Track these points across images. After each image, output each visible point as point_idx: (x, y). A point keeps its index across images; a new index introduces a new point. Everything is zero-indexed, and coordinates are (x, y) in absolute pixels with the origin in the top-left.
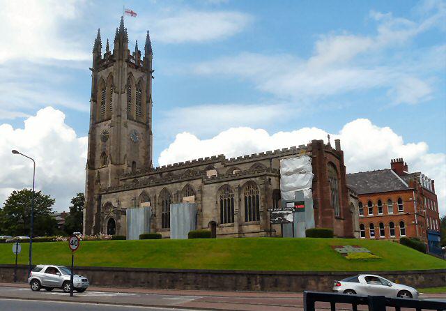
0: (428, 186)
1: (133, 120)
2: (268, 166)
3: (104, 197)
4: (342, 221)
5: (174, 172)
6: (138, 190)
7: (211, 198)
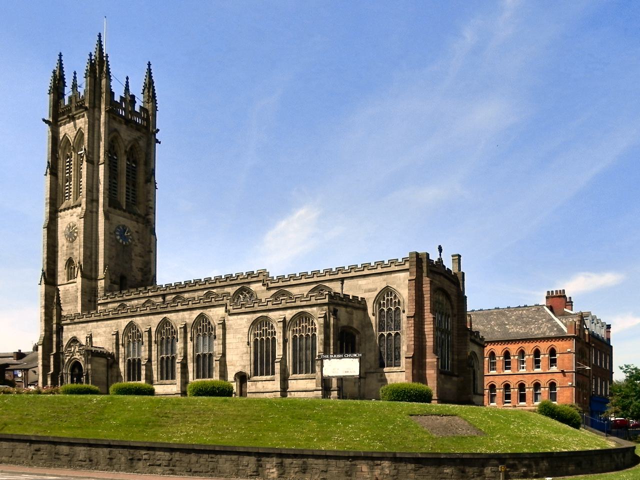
0: (602, 333)
1: (120, 208)
2: (338, 290)
4: (455, 379)
5: (186, 295)
6: (122, 320)
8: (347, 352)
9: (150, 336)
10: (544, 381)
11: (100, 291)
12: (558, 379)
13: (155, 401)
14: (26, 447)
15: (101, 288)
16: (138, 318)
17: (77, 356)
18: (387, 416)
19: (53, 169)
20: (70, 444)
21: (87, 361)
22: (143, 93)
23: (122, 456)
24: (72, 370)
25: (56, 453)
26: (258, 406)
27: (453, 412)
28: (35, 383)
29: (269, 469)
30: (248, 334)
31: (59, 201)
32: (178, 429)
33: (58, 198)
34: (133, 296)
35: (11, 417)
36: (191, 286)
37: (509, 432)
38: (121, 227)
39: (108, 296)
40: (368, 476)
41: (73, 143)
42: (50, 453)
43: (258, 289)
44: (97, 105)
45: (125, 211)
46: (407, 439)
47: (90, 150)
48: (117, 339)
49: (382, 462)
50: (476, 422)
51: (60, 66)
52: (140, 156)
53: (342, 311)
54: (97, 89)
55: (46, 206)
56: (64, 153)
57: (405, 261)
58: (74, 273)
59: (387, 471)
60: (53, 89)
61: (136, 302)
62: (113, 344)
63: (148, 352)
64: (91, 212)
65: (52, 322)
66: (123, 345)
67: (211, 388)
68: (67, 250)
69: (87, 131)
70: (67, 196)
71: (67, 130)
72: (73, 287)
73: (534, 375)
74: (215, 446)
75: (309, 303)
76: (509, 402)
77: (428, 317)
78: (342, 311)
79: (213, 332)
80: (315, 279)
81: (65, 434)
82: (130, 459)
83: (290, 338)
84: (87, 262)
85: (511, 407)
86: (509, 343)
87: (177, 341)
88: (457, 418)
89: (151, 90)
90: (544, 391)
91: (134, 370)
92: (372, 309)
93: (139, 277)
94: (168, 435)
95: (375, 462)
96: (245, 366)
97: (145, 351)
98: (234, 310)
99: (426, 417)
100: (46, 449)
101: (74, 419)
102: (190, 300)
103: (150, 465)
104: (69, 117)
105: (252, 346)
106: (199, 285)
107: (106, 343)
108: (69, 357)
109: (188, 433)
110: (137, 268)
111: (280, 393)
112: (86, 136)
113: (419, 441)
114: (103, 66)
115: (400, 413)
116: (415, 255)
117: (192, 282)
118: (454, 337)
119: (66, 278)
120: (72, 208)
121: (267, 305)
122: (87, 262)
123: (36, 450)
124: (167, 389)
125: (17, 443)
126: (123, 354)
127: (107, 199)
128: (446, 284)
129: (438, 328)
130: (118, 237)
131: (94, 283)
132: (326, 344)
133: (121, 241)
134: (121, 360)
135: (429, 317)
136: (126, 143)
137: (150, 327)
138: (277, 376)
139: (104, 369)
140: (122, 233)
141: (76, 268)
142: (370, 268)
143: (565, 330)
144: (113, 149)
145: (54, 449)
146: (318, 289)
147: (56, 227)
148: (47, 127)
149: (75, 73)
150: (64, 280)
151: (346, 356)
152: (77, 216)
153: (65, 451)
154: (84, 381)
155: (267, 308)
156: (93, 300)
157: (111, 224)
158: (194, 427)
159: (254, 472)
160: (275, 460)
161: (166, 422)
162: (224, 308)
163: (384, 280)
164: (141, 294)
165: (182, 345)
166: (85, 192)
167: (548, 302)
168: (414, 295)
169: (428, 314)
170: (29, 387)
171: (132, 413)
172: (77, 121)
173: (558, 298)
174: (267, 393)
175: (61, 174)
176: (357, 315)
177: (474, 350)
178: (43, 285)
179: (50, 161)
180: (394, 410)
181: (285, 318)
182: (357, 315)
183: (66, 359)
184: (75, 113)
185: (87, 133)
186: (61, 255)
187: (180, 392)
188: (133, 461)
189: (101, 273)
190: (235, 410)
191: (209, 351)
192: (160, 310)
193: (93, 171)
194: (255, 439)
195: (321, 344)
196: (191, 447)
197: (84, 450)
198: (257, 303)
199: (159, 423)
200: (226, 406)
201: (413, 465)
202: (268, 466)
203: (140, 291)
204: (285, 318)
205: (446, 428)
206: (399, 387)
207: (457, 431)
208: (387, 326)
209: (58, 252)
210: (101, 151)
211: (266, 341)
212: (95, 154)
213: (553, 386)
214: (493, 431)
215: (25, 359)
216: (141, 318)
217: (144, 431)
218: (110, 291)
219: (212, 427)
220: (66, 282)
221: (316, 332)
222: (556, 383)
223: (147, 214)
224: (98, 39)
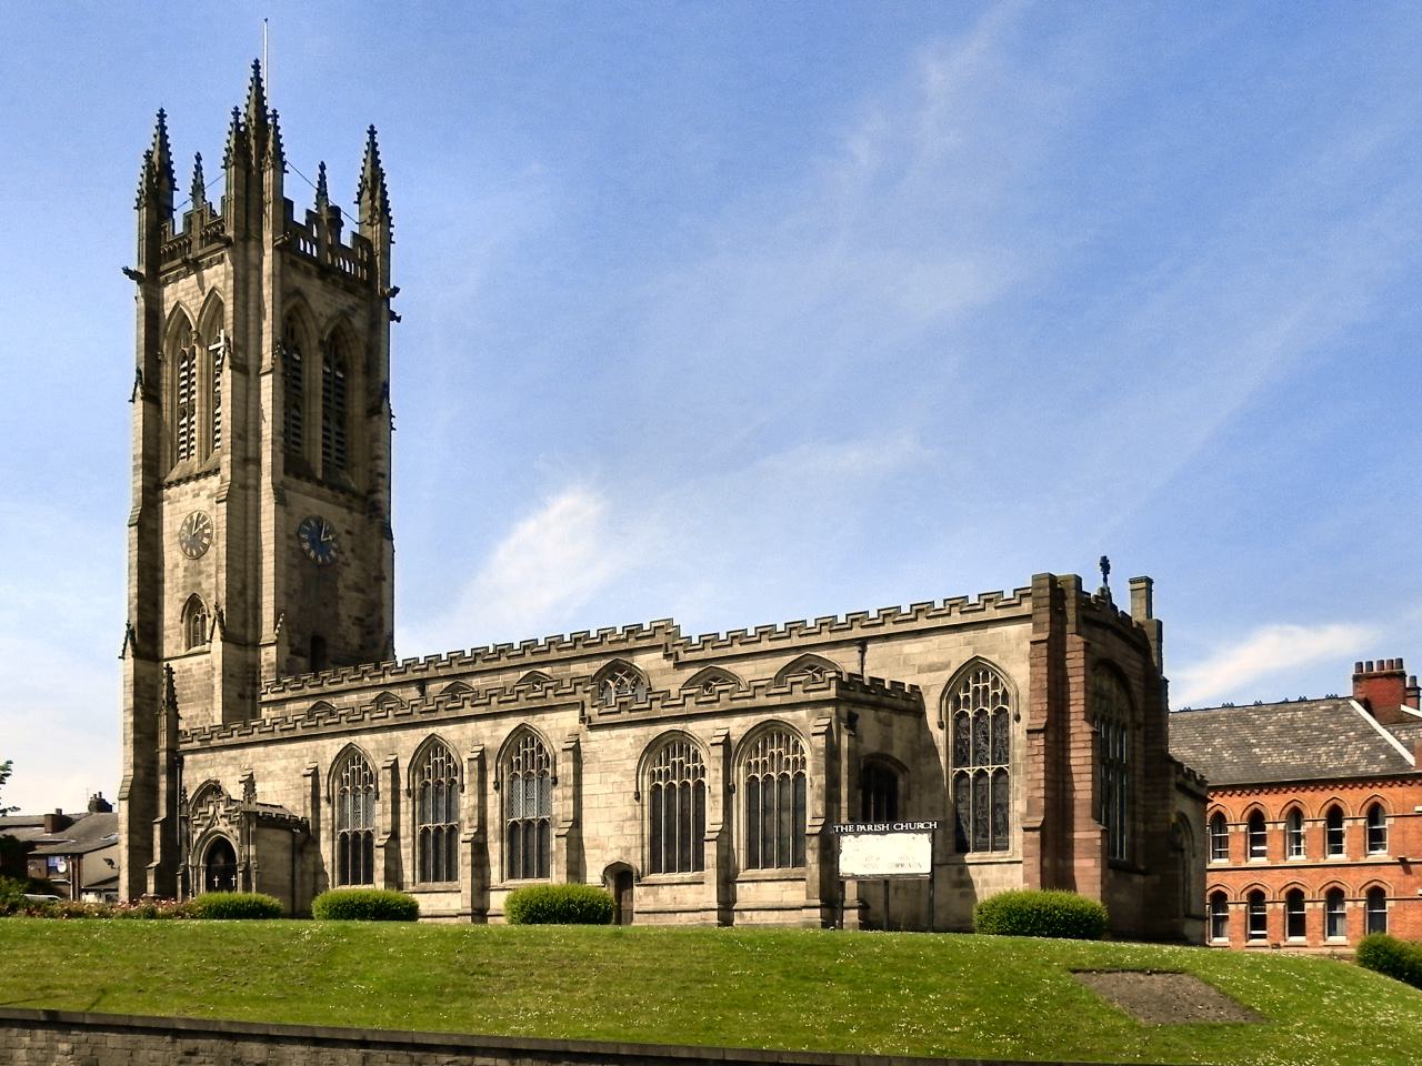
1: (310, 478)
4: (1138, 879)
5: (476, 682)
6: (327, 742)
7: (617, 778)
8: (878, 820)
9: (395, 779)
10: (1354, 884)
11: (266, 672)
12: (1391, 880)
13: (449, 935)
15: (268, 665)
17: (222, 826)
18: (1017, 974)
19: (149, 386)
20: (269, 1039)
21: (246, 839)
22: (358, 202)
24: (210, 858)
25: (234, 1060)
26: (699, 948)
27: (1175, 963)
28: (106, 887)
30: (637, 775)
32: (516, 1004)
33: (162, 453)
34: (346, 685)
35: (115, 973)
37: (1324, 1015)
39: (286, 684)
43: (653, 667)
44: (253, 233)
45: (320, 483)
46: (1076, 1029)
47: (240, 342)
48: (316, 787)
50: (1236, 988)
51: (161, 142)
53: (867, 718)
54: (254, 195)
55: (135, 475)
57: (1021, 595)
58: (203, 629)
60: (147, 197)
61: (353, 698)
62: (305, 797)
63: (390, 815)
64: (245, 487)
65: (157, 747)
66: (328, 800)
68: (184, 576)
69: (231, 295)
70: (183, 450)
71: (182, 294)
72: (199, 664)
73: (1327, 870)
74: (618, 1045)
75: (788, 700)
76: (1263, 936)
77: (1080, 731)
78: (867, 718)
79: (550, 770)
80: (796, 641)
81: (250, 1014)
83: (741, 783)
84: (235, 605)
85: (1266, 947)
86: (1261, 791)
87: (463, 791)
88: (1186, 979)
89: (378, 194)
90: (1354, 909)
91: (356, 858)
92: (936, 713)
93: (355, 638)
94: (496, 1018)
96: (629, 849)
97: (384, 813)
98: (603, 717)
99: (1111, 975)
100: (212, 1051)
101: (263, 979)
102: (495, 695)
104: (186, 262)
105: (646, 803)
106: (509, 657)
107: (287, 795)
108: (203, 830)
109: (543, 1014)
110: (350, 617)
111: (716, 913)
112: (229, 308)
113: (1106, 1034)
114: (267, 139)
115: (1046, 965)
116: (1047, 582)
117: (491, 651)
118: (1137, 779)
119: (183, 643)
120: (197, 477)
121: (684, 704)
122: (235, 605)
123: (188, 1053)
124: (443, 903)
125: (143, 1037)
127: (281, 456)
128: (1119, 650)
129: (1103, 760)
130: (306, 546)
131: (250, 653)
132: (831, 797)
133: (312, 554)
134: (323, 835)
135: (1082, 732)
136: (323, 322)
137: (395, 757)
138: (710, 873)
139: (286, 856)
140: (315, 537)
141: (209, 622)
142: (932, 614)
143: (1411, 759)
144: (293, 337)
145: (230, 1051)
146: (801, 663)
147: (157, 524)
148: (134, 288)
149: (198, 158)
150: (178, 647)
151: (897, 827)
152: (210, 497)
153: (256, 1055)
154: (240, 885)
156: (249, 693)
157: (290, 514)
158: (555, 998)
161: (485, 987)
162: (577, 713)
163: (969, 644)
164: (367, 679)
165: (474, 800)
166: (229, 440)
167: (1359, 690)
168: (1046, 677)
169: (1079, 723)
170: (84, 896)
171: (399, 965)
172: (206, 272)
173: (1384, 679)
174: (684, 914)
175: (169, 398)
176: (902, 726)
177: (1183, 810)
178: (130, 660)
179: (142, 367)
180: (1030, 958)
181: (727, 736)
182: (901, 727)
184: (200, 253)
185: (231, 301)
186: (172, 588)
187: (470, 910)
189: (268, 631)
190: (645, 958)
191: (541, 811)
192: (419, 719)
193: (247, 390)
194: (708, 1028)
195: (819, 797)
196: (560, 1048)
197: (303, 1053)
198: (658, 699)
199: (468, 989)
200: (622, 948)
203: (365, 672)
204: (727, 736)
205: (1164, 1004)
206: (1023, 903)
207: (1195, 1010)
208: (976, 753)
209: (163, 581)
211: (681, 790)
213: (1376, 896)
214: (1282, 1013)
215: (71, 830)
217: (438, 1008)
218: (289, 674)
219: (596, 999)
220: (183, 652)
221: (804, 768)
222: (1386, 888)
223: (373, 491)
224: (252, 75)
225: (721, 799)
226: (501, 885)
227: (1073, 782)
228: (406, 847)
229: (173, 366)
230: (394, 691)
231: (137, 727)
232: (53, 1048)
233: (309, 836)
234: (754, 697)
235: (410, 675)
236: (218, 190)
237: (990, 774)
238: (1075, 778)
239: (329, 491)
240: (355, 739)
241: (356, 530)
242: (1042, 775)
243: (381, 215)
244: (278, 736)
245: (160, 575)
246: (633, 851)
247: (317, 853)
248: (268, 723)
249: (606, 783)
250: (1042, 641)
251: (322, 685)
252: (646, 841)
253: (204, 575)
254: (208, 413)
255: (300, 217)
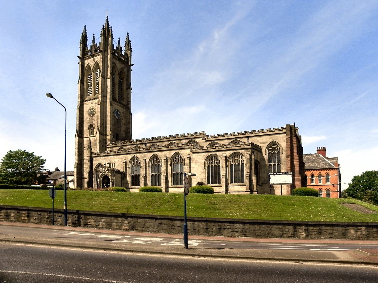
1: (116, 101)
3: (96, 159)
5: (158, 144)
6: (129, 155)
7: (200, 164)
9: (146, 164)
12: (331, 188)
14: (153, 222)
16: (138, 154)
17: (107, 173)
19: (82, 80)
21: (113, 176)
22: (125, 47)
23: (214, 227)
24: (103, 180)
29: (301, 232)
31: (85, 96)
33: (84, 95)
34: (127, 144)
36: (161, 139)
38: (116, 110)
40: (354, 235)
41: (93, 68)
42: (168, 226)
43: (200, 141)
44: (106, 50)
45: (118, 102)
47: (103, 72)
48: (126, 165)
49: (362, 228)
52: (124, 76)
54: (107, 42)
56: (87, 73)
59: (364, 233)
61: (129, 147)
62: (124, 167)
64: (103, 102)
67: (205, 190)
70: (89, 94)
71: (89, 62)
72: (93, 139)
80: (233, 137)
82: (219, 229)
87: (162, 166)
89: (129, 45)
91: (135, 180)
95: (358, 228)
97: (143, 171)
100: (166, 223)
103: (231, 232)
106: (166, 139)
108: (102, 173)
119: (89, 134)
120: (92, 99)
123: (160, 224)
124: (135, 190)
125: (148, 220)
126: (129, 172)
130: (115, 115)
134: (128, 175)
136: (119, 69)
139: (120, 180)
146: (234, 141)
148: (79, 60)
152: (95, 104)
153: (178, 224)
155: (216, 150)
156: (104, 145)
159: (292, 234)
160: (304, 228)
162: (190, 150)
163: (271, 138)
164: (132, 143)
165: (165, 168)
178: (77, 138)
179: (80, 76)
183: (100, 174)
184: (94, 54)
186: (86, 123)
188: (221, 230)
191: (138, 173)
192: (151, 151)
193: (104, 82)
196: (256, 221)
197: (190, 223)
201: (376, 229)
202: (300, 231)
209: (84, 121)
210: (108, 72)
212: (106, 73)
213: (328, 191)
216: (140, 154)
225: (225, 169)
226: (171, 187)
227: (295, 166)
228: (148, 178)
229: (87, 77)
230: (139, 145)
231: (78, 152)
232: (123, 223)
233: (125, 176)
234: (232, 147)
235: (143, 142)
236: (98, 41)
237: (277, 165)
238: (295, 166)
239: (119, 104)
240: (135, 155)
241: (124, 112)
242: (290, 165)
243: (130, 49)
244: (117, 154)
245: (83, 120)
246: (203, 180)
247: (126, 179)
248: (114, 151)
249: (197, 165)
250: (289, 138)
251: (121, 144)
252: (206, 177)
253: (94, 120)
254: (95, 87)
255: (115, 48)
